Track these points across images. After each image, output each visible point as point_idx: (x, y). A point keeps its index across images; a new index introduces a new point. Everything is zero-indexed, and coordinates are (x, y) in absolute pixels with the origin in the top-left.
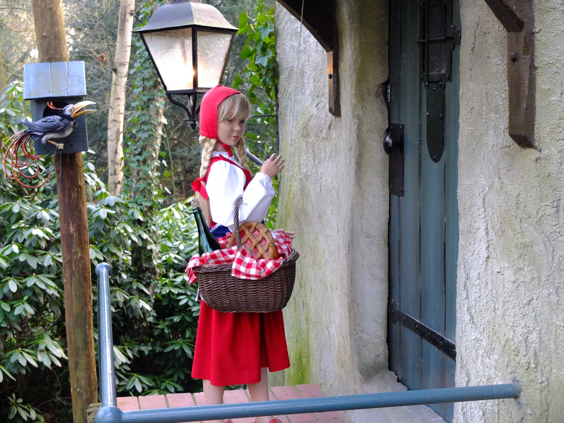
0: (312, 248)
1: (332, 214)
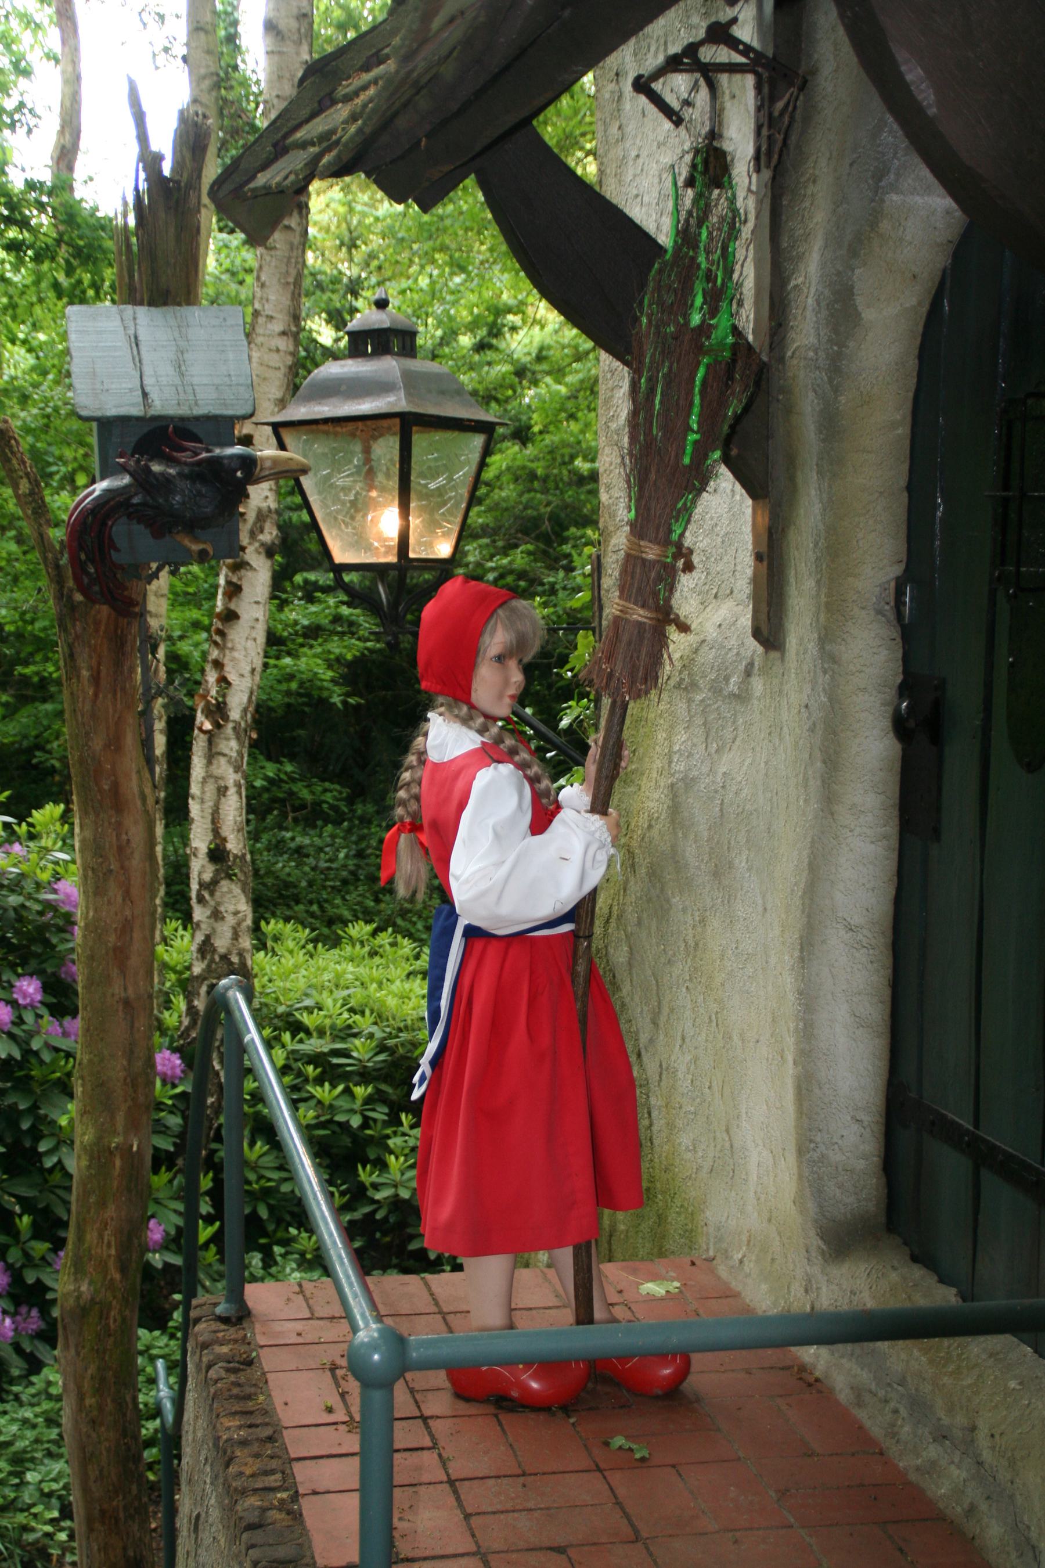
0: (691, 943)
1: (749, 869)
